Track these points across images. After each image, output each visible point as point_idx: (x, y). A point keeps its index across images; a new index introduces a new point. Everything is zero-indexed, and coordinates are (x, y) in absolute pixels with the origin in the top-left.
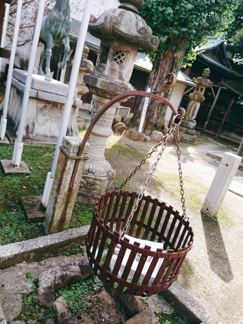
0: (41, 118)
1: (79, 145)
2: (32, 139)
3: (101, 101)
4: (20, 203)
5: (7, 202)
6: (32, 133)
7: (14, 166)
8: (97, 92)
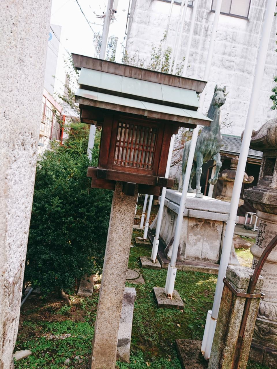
0: (192, 238)
1: (249, 278)
2: (183, 261)
3: (270, 218)
4: (175, 347)
5: (161, 343)
6: (183, 254)
7: (168, 296)
8: (264, 209)
